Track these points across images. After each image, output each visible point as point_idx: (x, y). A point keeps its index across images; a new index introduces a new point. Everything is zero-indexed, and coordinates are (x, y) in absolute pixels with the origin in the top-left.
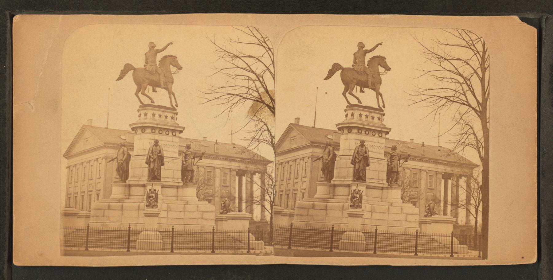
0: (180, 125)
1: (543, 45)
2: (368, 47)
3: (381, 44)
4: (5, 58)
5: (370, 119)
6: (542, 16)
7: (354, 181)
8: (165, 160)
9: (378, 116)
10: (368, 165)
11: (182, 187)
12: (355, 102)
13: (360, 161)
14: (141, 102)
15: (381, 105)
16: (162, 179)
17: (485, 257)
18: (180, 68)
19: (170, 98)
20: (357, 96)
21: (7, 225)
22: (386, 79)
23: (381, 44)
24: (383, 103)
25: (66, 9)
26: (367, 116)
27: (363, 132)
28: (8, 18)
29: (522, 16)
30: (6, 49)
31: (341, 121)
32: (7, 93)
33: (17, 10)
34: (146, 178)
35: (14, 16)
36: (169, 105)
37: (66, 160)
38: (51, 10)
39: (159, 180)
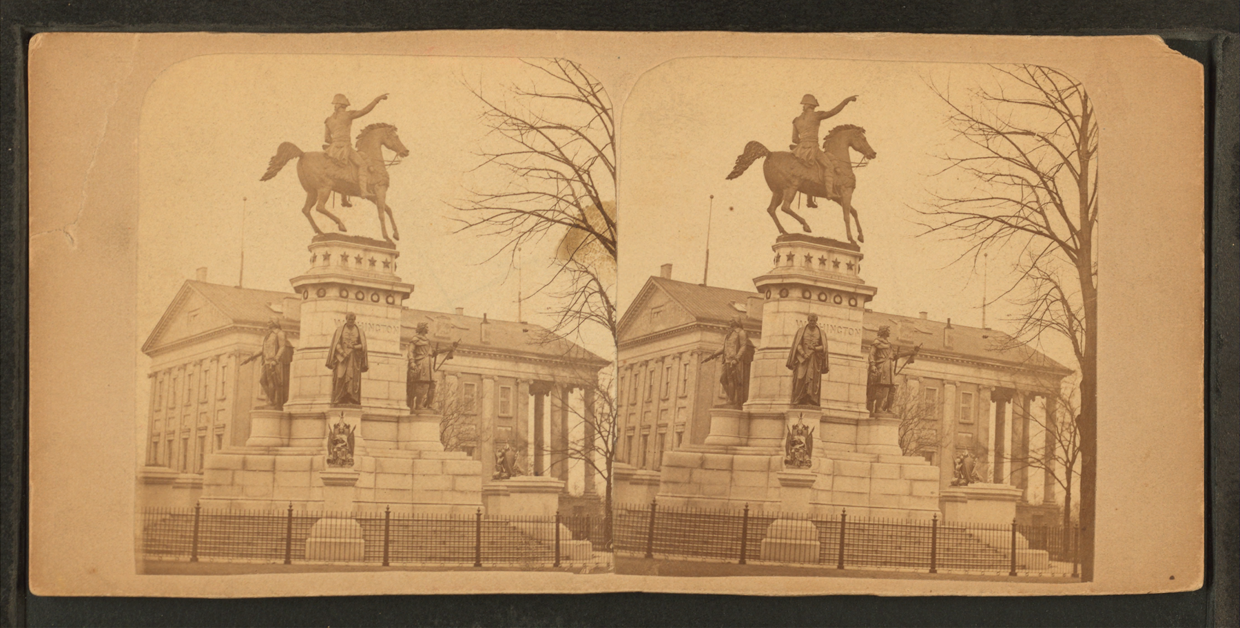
0: (404, 281)
1: (1218, 102)
2: (824, 106)
3: (854, 99)
4: (12, 131)
5: (829, 266)
6: (1216, 37)
7: (793, 405)
8: (371, 358)
9: (848, 259)
10: (826, 370)
11: (409, 419)
12: (334, 229)
13: (807, 361)
14: (317, 230)
15: (855, 235)
18: (404, 153)
19: (382, 220)
20: (801, 215)
21: (16, 505)
22: (864, 175)
23: (854, 99)
25: (147, 21)
26: (822, 261)
27: (814, 297)
28: (19, 41)
30: (13, 110)
31: (765, 272)
32: (16, 209)
33: (38, 23)
35: (31, 35)
36: (378, 237)
37: (148, 359)
39: (357, 403)
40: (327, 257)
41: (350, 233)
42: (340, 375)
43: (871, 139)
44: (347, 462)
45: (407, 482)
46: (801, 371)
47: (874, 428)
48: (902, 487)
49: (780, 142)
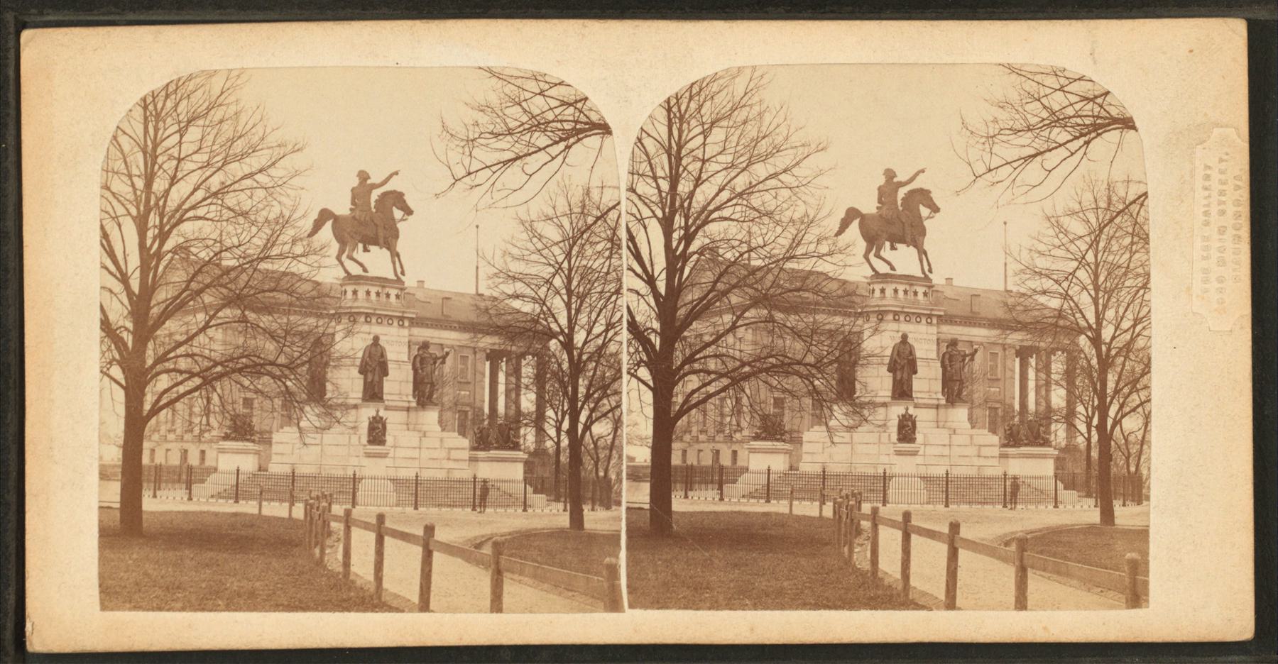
2: (901, 177)
3: (396, 173)
5: (383, 297)
7: (893, 397)
8: (391, 366)
10: (915, 372)
11: (416, 409)
13: (903, 367)
16: (385, 397)
19: (394, 263)
22: (932, 226)
23: (396, 173)
24: (929, 264)
27: (374, 320)
34: (360, 395)
36: (391, 276)
39: (381, 399)
40: (883, 291)
41: (899, 272)
42: (899, 377)
45: (946, 451)
46: (899, 374)
47: (421, 413)
48: (971, 451)
49: (869, 206)
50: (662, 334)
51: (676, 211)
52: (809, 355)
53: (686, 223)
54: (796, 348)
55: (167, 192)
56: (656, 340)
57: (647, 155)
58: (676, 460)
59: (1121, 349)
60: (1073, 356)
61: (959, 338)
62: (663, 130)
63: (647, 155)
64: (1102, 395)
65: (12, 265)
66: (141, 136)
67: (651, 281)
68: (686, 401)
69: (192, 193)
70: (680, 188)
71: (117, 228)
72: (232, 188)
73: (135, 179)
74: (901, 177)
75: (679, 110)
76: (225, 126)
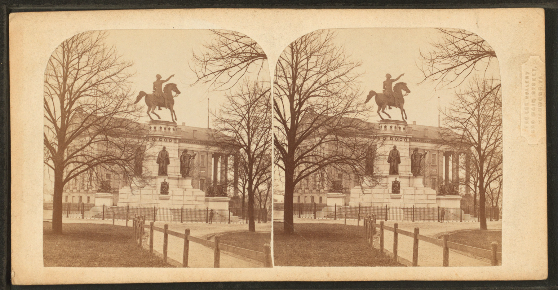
2: (393, 77)
3: (173, 76)
8: (170, 160)
13: (394, 160)
17: (496, 260)
20: (157, 113)
21: (5, 229)
23: (173, 76)
26: (165, 128)
27: (163, 140)
28: (5, 13)
29: (546, 7)
30: (3, 45)
33: (14, 5)
38: (50, 4)
40: (385, 127)
41: (392, 119)
42: (392, 165)
43: (409, 86)
44: (398, 192)
47: (184, 180)
50: (289, 146)
51: (295, 92)
52: (353, 155)
53: (300, 97)
54: (347, 152)
55: (73, 84)
56: (286, 149)
57: (283, 68)
58: (295, 201)
59: (489, 152)
60: (468, 155)
61: (419, 148)
62: (290, 57)
63: (283, 68)
64: (481, 172)
65: (5, 115)
66: (62, 59)
67: (284, 123)
68: (300, 175)
69: (84, 84)
70: (297, 82)
71: (51, 99)
72: (101, 82)
73: (59, 78)
74: (393, 77)
75: (68, 47)
76: (98, 55)
